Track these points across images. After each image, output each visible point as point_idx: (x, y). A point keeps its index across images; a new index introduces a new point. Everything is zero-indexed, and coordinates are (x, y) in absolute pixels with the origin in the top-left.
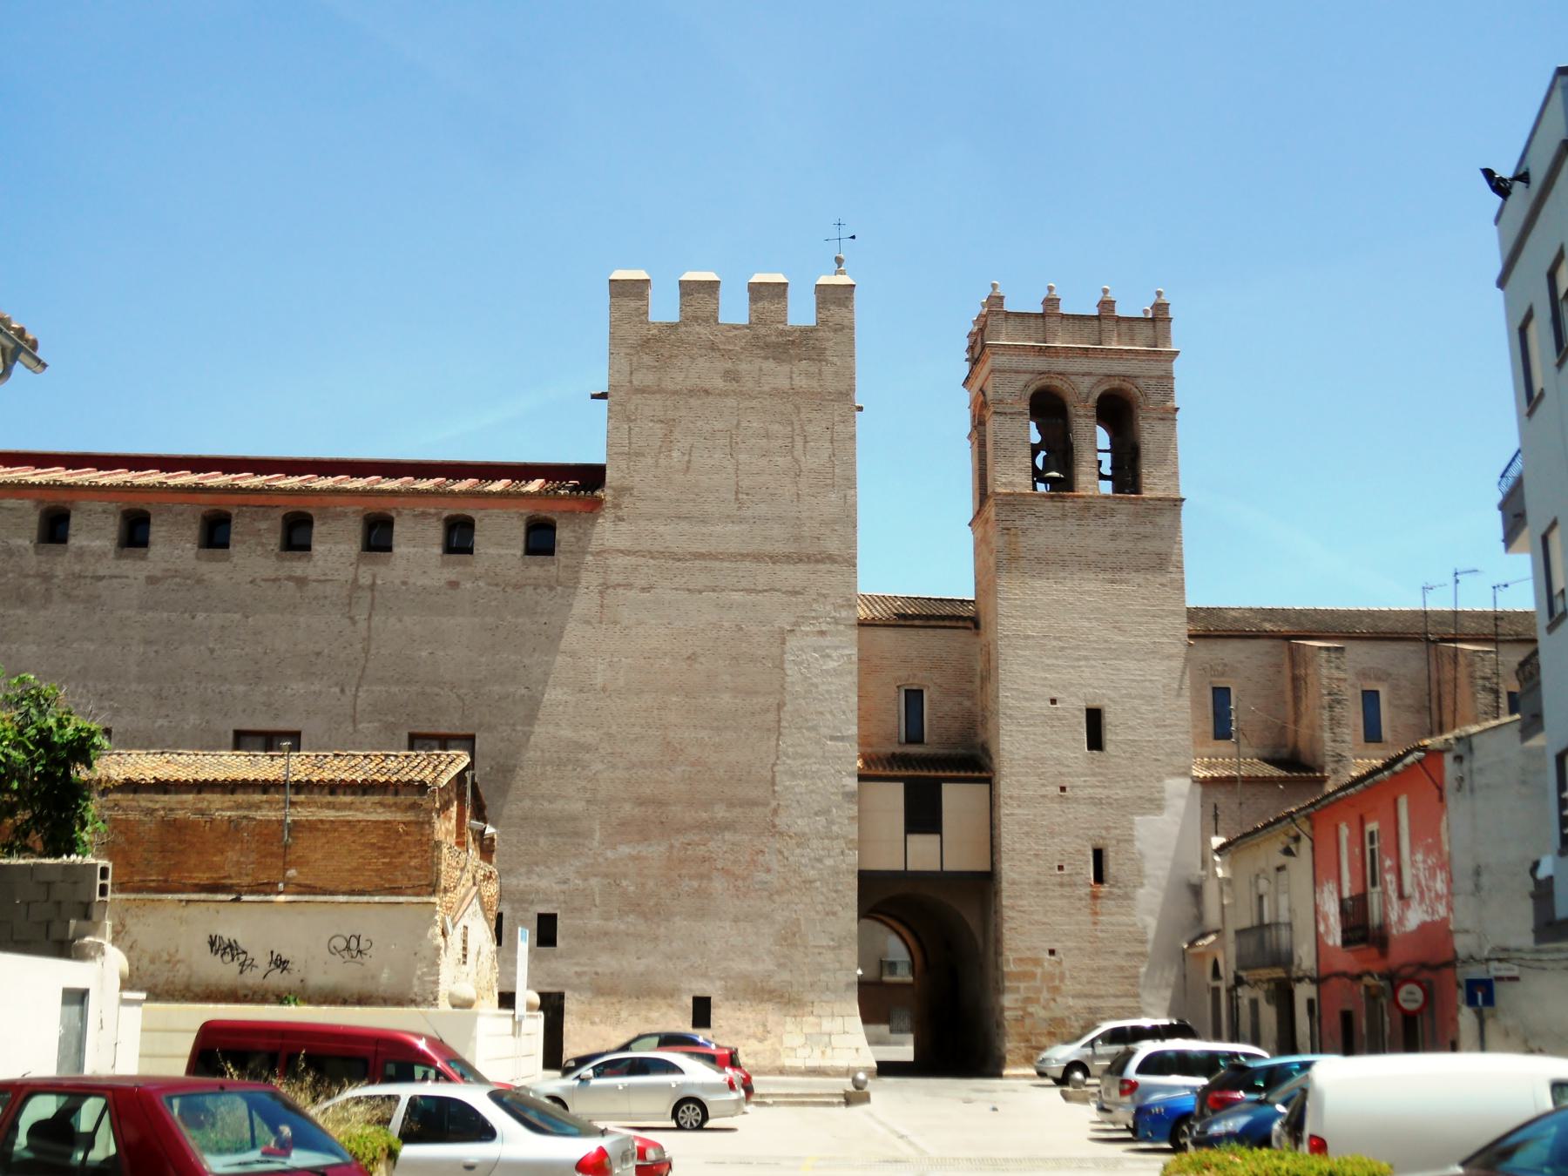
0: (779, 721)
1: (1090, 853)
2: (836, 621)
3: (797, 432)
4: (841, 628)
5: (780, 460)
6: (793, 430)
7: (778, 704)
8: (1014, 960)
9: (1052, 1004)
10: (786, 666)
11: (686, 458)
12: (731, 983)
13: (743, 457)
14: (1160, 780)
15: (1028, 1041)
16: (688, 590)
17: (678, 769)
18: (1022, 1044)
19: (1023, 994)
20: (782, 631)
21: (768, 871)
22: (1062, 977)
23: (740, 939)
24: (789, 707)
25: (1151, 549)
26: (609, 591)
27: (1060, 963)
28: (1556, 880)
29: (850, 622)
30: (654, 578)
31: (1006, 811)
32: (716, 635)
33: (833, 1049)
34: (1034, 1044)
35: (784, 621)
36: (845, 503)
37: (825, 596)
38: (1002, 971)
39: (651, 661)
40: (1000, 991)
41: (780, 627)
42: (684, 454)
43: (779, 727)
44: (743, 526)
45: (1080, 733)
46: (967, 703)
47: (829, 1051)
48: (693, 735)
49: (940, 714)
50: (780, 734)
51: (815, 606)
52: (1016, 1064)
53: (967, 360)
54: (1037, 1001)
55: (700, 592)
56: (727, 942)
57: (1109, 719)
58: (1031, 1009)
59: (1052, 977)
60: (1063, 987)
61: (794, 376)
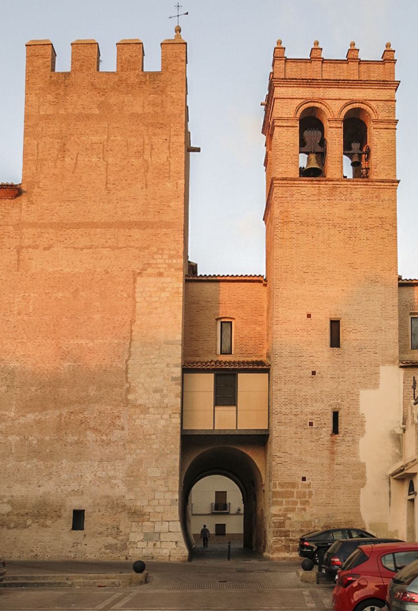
0: (132, 331)
2: (170, 266)
4: (173, 270)
7: (130, 321)
8: (279, 483)
10: (136, 295)
12: (98, 501)
13: (110, 160)
14: (378, 366)
16: (74, 248)
17: (67, 364)
19: (284, 506)
21: (123, 429)
22: (310, 494)
24: (138, 322)
25: (376, 215)
30: (53, 241)
33: (161, 542)
35: (137, 266)
37: (162, 249)
39: (50, 295)
47: (158, 543)
49: (241, 336)
51: (155, 256)
54: (293, 510)
55: (82, 249)
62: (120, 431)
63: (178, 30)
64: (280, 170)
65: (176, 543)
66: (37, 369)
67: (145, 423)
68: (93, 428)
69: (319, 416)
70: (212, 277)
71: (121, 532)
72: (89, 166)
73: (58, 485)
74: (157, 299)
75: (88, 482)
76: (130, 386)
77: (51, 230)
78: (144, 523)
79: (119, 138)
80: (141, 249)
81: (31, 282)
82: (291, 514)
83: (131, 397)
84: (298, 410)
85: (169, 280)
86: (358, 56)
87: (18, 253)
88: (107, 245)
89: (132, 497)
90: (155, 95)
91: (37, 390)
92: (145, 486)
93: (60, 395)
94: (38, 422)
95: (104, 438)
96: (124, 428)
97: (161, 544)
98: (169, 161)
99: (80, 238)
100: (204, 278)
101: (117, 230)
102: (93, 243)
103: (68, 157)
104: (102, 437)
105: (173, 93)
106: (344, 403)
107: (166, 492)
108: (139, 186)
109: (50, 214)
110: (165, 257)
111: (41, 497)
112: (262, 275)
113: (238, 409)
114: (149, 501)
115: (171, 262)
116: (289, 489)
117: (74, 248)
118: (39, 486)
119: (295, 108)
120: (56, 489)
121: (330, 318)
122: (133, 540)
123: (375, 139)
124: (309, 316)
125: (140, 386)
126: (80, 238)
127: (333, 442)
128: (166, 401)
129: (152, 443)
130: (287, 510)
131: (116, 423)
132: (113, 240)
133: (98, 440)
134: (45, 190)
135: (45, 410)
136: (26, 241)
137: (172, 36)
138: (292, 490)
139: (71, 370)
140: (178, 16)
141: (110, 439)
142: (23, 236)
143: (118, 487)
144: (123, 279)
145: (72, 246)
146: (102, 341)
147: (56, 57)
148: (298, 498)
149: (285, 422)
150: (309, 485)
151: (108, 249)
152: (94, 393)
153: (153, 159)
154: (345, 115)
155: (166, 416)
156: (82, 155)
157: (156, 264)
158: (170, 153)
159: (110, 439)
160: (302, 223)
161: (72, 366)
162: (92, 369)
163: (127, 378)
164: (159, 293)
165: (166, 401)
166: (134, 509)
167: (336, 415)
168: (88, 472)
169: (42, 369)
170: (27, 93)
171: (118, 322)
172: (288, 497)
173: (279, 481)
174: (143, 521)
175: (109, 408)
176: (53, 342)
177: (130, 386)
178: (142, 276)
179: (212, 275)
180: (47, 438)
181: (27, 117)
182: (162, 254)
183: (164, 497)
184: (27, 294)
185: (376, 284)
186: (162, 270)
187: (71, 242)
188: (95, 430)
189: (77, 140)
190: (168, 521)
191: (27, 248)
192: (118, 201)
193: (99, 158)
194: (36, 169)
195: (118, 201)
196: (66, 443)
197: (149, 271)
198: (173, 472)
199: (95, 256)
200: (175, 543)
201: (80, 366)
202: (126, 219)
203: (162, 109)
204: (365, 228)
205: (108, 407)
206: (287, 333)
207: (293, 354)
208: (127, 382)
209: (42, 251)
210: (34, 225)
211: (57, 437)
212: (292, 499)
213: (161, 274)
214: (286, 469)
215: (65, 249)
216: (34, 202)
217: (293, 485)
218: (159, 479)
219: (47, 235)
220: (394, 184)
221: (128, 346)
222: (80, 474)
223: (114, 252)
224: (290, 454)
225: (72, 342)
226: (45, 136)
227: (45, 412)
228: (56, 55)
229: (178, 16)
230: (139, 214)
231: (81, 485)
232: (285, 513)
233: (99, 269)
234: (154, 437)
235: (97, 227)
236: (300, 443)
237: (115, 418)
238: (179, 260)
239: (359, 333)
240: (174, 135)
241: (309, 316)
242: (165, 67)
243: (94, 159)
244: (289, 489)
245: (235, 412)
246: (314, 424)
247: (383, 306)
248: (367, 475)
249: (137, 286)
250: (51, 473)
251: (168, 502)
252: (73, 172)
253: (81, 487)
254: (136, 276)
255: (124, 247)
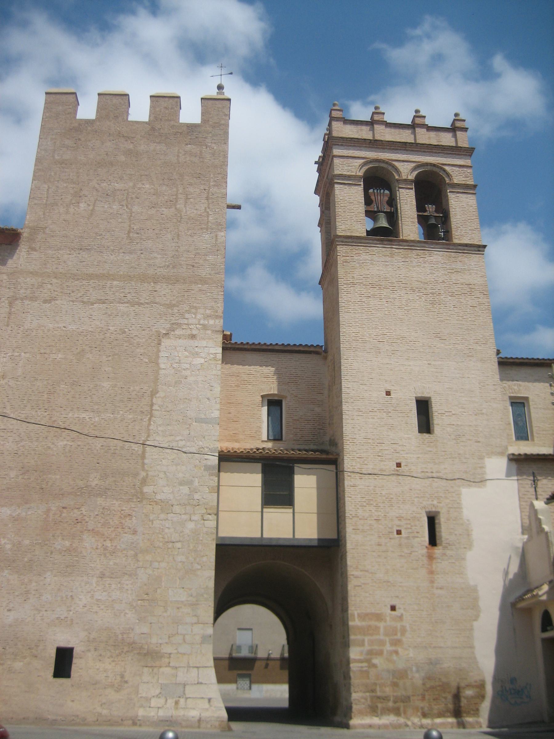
0: (152, 405)
1: (426, 519)
2: (205, 327)
3: (180, 191)
4: (209, 332)
5: (166, 211)
6: (178, 190)
7: (152, 392)
8: (358, 615)
9: (395, 657)
10: (160, 361)
11: (91, 208)
12: (94, 635)
13: (136, 209)
14: (481, 458)
15: (373, 691)
16: (83, 302)
17: (61, 443)
18: (368, 694)
19: (367, 647)
20: (159, 334)
21: (135, 532)
22: (403, 631)
23: (104, 593)
24: (161, 394)
25: (462, 281)
26: (17, 302)
27: (401, 617)
28: (345, 731)
29: (217, 329)
30: (56, 293)
31: (348, 482)
32: (102, 337)
33: (187, 698)
34: (379, 694)
35: (162, 326)
36: (216, 241)
37: (196, 308)
38: (348, 625)
39: (46, 356)
40: (346, 645)
41: (157, 331)
42: (89, 205)
43: (152, 410)
44: (132, 256)
45: (415, 415)
46: (317, 409)
47: (182, 701)
48: (76, 416)
49: (295, 418)
50: (152, 416)
51: (187, 316)
52: (362, 713)
53: (316, 163)
54: (380, 653)
55: (92, 304)
56: (92, 597)
57: (436, 408)
58: (375, 661)
59: (394, 631)
60: (404, 639)
61: (180, 155)
62: (130, 536)
63: (220, 87)
64: (343, 227)
65: (210, 700)
66: (21, 448)
67: (167, 526)
68: (93, 530)
69: (408, 522)
70: (244, 344)
71: (126, 682)
72: (110, 213)
73: (37, 609)
74: (187, 366)
75: (81, 607)
76: (147, 474)
77: (55, 281)
78: (162, 670)
79: (147, 186)
80: (171, 306)
81: (24, 340)
82: (376, 658)
83: (146, 489)
84: (380, 513)
85: (204, 343)
86: (425, 122)
87: (11, 304)
88: (126, 300)
89: (145, 630)
90: (193, 146)
91: (17, 476)
92: (165, 614)
93: (50, 484)
94: (16, 519)
95: (108, 544)
96: (136, 531)
97: (186, 701)
98: (208, 212)
99: (91, 290)
100: (246, 347)
101: (140, 283)
102: (107, 298)
103: (84, 203)
104: (104, 543)
105: (214, 145)
106: (441, 505)
107: (195, 623)
108: (169, 236)
109: (56, 262)
110: (199, 316)
111: (10, 626)
112: (321, 345)
113: (296, 511)
114: (169, 637)
115: (207, 323)
116: (373, 623)
117: (83, 302)
118: (9, 610)
119: (358, 167)
120: (34, 615)
121: (416, 397)
122: (144, 695)
123: (453, 202)
124: (388, 393)
125: (162, 475)
126: (91, 290)
127: (431, 558)
128: (197, 496)
129: (176, 553)
130: (370, 652)
131: (126, 524)
132: (134, 295)
133: (99, 547)
134: (53, 236)
135: (26, 503)
136: (22, 291)
137: (213, 92)
138: (377, 623)
139: (67, 451)
140: (221, 75)
141: (116, 546)
142: (19, 286)
143: (125, 615)
144: (144, 340)
145: (80, 299)
146: (112, 416)
147: (79, 107)
148: (386, 634)
149: (363, 530)
150: (401, 617)
151: (127, 305)
152: (96, 482)
153: (188, 209)
154: (416, 176)
155: (196, 517)
156: (102, 201)
157: (187, 324)
158: (209, 204)
159: (116, 546)
160: (373, 286)
161: (69, 447)
162: (95, 452)
163: (143, 464)
164: (190, 359)
165: (197, 496)
166: (146, 647)
167: (432, 521)
168: (82, 592)
169: (27, 448)
170: (42, 137)
171: (135, 393)
172: (372, 635)
173: (359, 611)
174: (161, 667)
175: (117, 503)
176: (46, 414)
177: (147, 474)
178: (169, 338)
179: (245, 343)
180: (27, 542)
181: (39, 161)
182: (195, 314)
183: (192, 631)
184: (17, 354)
185: (471, 358)
186: (194, 332)
187: (80, 295)
188: (94, 532)
189: (96, 186)
190: (198, 667)
191: (22, 300)
192: (142, 252)
193: (123, 206)
194: (44, 214)
195: (142, 252)
196: (53, 549)
197: (178, 332)
198: (205, 596)
199: (109, 313)
200: (207, 701)
201: (79, 446)
202: (151, 272)
203: (201, 160)
204: (450, 294)
205: (115, 502)
206: (360, 413)
207: (370, 441)
208: (143, 469)
209: (42, 304)
210: (34, 274)
211: (40, 542)
212: (377, 637)
213: (193, 337)
214: (367, 595)
215: (71, 303)
216: (37, 249)
217: (379, 617)
218: (185, 605)
219: (49, 286)
220: (480, 249)
221: (147, 423)
222: (71, 594)
223: (134, 308)
224: (372, 573)
225: (70, 415)
226: (58, 181)
227: (28, 506)
228: (79, 104)
229: (221, 75)
230: (168, 266)
231: (70, 611)
232: (369, 657)
233: (114, 328)
234: (179, 545)
235: (113, 280)
236: (385, 558)
237: (125, 516)
238: (217, 321)
239: (454, 416)
240: (214, 185)
241: (388, 393)
242: (205, 120)
243: (116, 207)
244: (373, 623)
245: (292, 515)
246: (403, 532)
247: (482, 384)
248: (481, 604)
249: (162, 348)
250: (27, 592)
251: (198, 638)
252: (88, 219)
253: (71, 613)
254: (161, 337)
255: (147, 303)
